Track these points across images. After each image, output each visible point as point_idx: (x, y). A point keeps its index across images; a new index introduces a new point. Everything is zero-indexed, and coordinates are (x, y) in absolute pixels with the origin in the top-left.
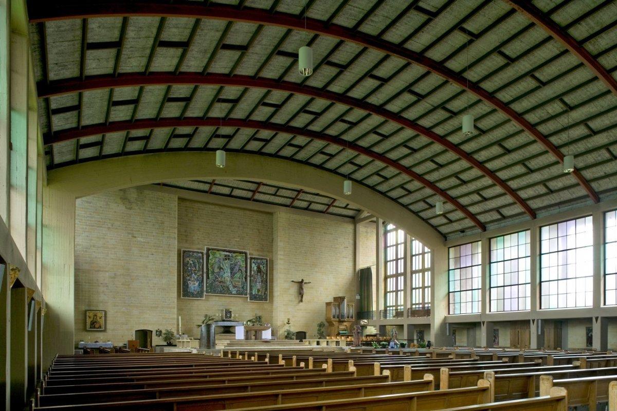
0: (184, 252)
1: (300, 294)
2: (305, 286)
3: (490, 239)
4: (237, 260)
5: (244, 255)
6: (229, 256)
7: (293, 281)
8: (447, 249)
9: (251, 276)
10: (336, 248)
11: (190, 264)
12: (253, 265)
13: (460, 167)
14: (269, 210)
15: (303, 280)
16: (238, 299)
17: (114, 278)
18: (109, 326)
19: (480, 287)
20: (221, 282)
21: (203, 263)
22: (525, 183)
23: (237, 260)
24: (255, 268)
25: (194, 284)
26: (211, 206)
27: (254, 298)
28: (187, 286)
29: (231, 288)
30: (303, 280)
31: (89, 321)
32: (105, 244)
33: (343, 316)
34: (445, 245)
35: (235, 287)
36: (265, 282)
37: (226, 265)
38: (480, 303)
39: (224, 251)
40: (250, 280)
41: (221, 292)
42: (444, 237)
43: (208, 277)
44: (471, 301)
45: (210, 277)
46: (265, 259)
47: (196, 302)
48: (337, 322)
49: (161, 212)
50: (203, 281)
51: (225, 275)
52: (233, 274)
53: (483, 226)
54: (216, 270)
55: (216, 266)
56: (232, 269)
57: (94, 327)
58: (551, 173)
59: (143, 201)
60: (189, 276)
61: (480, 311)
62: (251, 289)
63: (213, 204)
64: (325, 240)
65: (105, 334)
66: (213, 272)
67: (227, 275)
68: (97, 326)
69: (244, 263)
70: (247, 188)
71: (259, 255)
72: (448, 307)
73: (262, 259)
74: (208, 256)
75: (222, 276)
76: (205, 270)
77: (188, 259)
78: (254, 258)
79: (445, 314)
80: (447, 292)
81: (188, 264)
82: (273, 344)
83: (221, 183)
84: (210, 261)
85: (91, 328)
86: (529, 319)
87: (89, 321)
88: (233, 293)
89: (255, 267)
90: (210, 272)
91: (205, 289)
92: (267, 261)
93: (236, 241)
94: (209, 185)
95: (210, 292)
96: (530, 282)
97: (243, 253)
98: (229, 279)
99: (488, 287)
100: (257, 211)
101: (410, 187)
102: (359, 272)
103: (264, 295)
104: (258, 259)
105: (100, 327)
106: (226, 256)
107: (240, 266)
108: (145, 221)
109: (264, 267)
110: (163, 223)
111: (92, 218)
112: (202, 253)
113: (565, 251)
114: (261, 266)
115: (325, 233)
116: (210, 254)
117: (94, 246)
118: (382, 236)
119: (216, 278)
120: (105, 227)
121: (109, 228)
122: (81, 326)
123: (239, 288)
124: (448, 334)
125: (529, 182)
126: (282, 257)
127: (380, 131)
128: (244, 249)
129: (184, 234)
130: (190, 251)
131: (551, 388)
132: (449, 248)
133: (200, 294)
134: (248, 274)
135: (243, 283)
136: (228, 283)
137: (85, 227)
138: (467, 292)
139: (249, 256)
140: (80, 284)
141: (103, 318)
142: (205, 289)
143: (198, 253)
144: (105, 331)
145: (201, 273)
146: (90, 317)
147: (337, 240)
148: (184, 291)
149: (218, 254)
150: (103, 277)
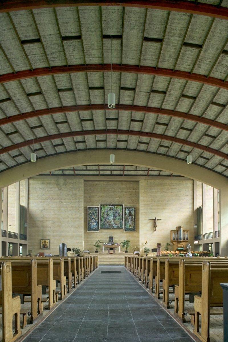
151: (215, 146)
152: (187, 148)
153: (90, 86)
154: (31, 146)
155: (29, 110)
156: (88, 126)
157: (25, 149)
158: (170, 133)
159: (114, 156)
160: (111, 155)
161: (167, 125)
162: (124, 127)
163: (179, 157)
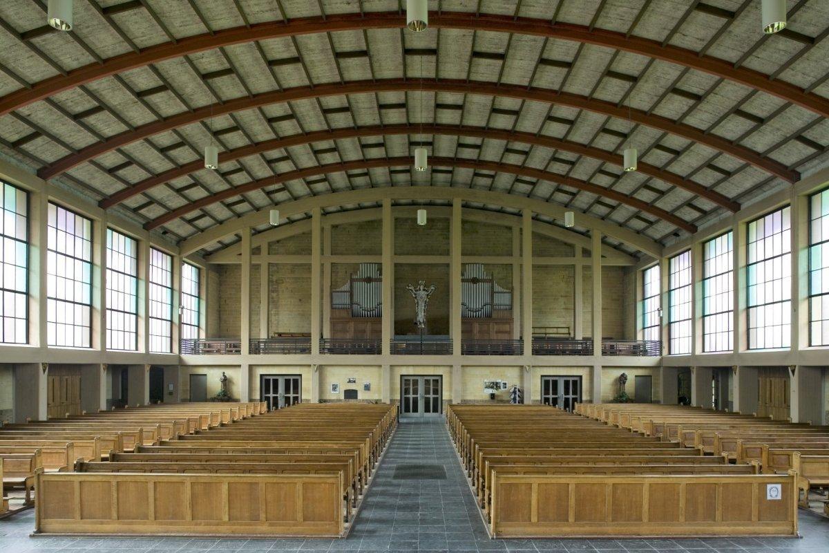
8: (805, 201)
14: (570, 241)
19: (691, 317)
38: (691, 338)
44: (823, 319)
53: (792, 174)
61: (732, 347)
86: (38, 362)
101: (755, 108)
113: (775, 255)
118: (299, 445)
127: (685, 88)
131: (46, 184)
138: (824, 296)
151: (699, 120)
152: (620, 124)
153: (365, 60)
154: (208, 121)
155: (197, 28)
156: (356, 70)
157: (192, 130)
158: (575, 88)
159: (425, 211)
160: (419, 212)
161: (569, 65)
162: (453, 70)
163: (607, 170)
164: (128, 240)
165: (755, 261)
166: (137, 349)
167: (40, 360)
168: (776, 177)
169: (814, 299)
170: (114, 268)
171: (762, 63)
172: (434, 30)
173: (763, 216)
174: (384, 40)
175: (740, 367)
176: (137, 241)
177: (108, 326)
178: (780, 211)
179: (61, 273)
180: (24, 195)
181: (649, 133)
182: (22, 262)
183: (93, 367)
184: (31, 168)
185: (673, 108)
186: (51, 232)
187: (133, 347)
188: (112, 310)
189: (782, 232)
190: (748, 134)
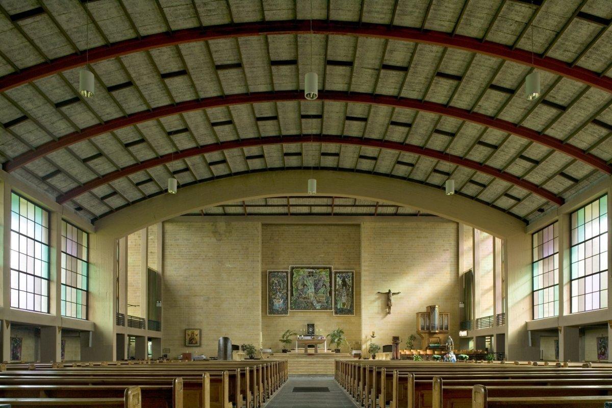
0: (270, 273)
1: (388, 305)
2: (393, 298)
3: (570, 215)
4: (321, 276)
5: (328, 270)
6: (312, 272)
7: (379, 292)
9: (335, 291)
10: (433, 252)
11: (276, 283)
12: (338, 279)
13: (476, 131)
15: (390, 291)
16: (323, 314)
17: (208, 301)
18: (204, 342)
20: (304, 298)
21: (288, 281)
22: (572, 128)
23: (321, 276)
24: (340, 282)
25: (280, 302)
26: (295, 227)
27: (339, 312)
28: (273, 304)
29: (315, 303)
30: (390, 291)
31: (188, 338)
32: (200, 273)
33: (433, 327)
34: (525, 231)
35: (318, 302)
36: (351, 295)
37: (310, 282)
39: (308, 268)
40: (335, 294)
41: (305, 308)
42: (525, 221)
43: (292, 295)
45: (294, 294)
46: (351, 272)
47: (282, 319)
48: (427, 334)
49: (246, 240)
50: (287, 298)
51: (310, 291)
52: (317, 290)
53: (559, 200)
54: (300, 287)
55: (300, 284)
56: (316, 285)
57: (192, 343)
58: (595, 102)
59: (230, 232)
60: (274, 294)
62: (336, 304)
63: (297, 225)
64: (418, 245)
65: (201, 349)
66: (297, 289)
67: (311, 291)
68: (194, 342)
69: (328, 278)
70: (324, 204)
71: (345, 269)
72: (531, 310)
73: (348, 272)
74: (292, 274)
75: (306, 292)
76: (289, 288)
77: (273, 279)
78: (339, 273)
79: (526, 318)
80: (529, 291)
81: (273, 283)
82: (317, 357)
83: (297, 204)
84: (294, 279)
85: (189, 344)
87: (188, 338)
88: (317, 308)
89: (339, 281)
90: (294, 290)
91: (289, 306)
92: (353, 274)
93: (321, 257)
94: (375, 208)
95: (295, 309)
96: (607, 268)
97: (327, 268)
98: (312, 295)
99: (566, 279)
100: (325, 225)
102: (462, 276)
103: (351, 309)
104: (343, 273)
105: (196, 343)
106: (309, 273)
107: (324, 281)
108: (232, 249)
109: (349, 280)
110: (248, 249)
111: (190, 252)
112: (287, 273)
114: (346, 279)
115: (417, 237)
116: (294, 273)
117: (192, 276)
119: (300, 295)
120: (200, 259)
121: (203, 259)
122: (183, 343)
123: (324, 303)
124: (530, 345)
125: (575, 124)
126: (367, 268)
128: (329, 264)
129: (268, 256)
130: (275, 272)
132: (533, 234)
133: (285, 311)
134: (333, 288)
135: (327, 298)
136: (312, 299)
137: (185, 260)
138: (593, 276)
139: (333, 271)
140: (182, 307)
141: (198, 335)
142: (289, 306)
143: (283, 272)
144: (200, 346)
145: (285, 291)
146: (189, 335)
147: (434, 243)
148: (269, 309)
149: (301, 272)
150: (199, 301)
152: (446, 166)
154: (168, 165)
158: (415, 141)
161: (409, 125)
164: (39, 210)
165: (576, 243)
166: (49, 312)
167: (58, 324)
168: (598, 170)
169: (573, 282)
170: (28, 236)
171: (534, 123)
172: (320, 102)
173: (584, 206)
174: (288, 109)
175: (564, 327)
176: (49, 213)
177: (63, 297)
178: (598, 200)
179: (23, 250)
180: (47, 213)
181: (465, 172)
182: (45, 258)
183: (51, 329)
184: (52, 197)
185: (478, 154)
186: (63, 240)
187: (45, 310)
188: (66, 285)
189: (599, 217)
190: (528, 171)
